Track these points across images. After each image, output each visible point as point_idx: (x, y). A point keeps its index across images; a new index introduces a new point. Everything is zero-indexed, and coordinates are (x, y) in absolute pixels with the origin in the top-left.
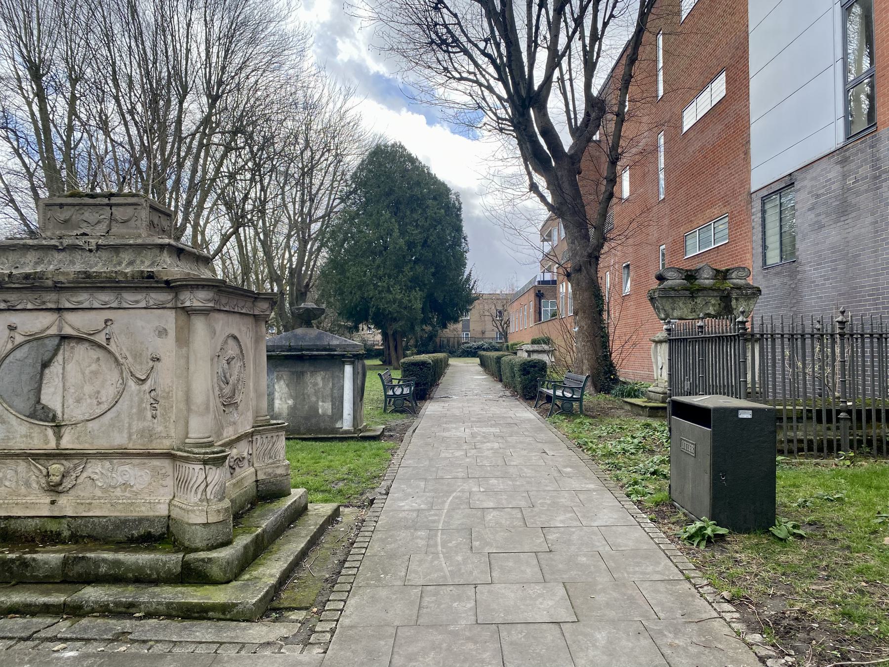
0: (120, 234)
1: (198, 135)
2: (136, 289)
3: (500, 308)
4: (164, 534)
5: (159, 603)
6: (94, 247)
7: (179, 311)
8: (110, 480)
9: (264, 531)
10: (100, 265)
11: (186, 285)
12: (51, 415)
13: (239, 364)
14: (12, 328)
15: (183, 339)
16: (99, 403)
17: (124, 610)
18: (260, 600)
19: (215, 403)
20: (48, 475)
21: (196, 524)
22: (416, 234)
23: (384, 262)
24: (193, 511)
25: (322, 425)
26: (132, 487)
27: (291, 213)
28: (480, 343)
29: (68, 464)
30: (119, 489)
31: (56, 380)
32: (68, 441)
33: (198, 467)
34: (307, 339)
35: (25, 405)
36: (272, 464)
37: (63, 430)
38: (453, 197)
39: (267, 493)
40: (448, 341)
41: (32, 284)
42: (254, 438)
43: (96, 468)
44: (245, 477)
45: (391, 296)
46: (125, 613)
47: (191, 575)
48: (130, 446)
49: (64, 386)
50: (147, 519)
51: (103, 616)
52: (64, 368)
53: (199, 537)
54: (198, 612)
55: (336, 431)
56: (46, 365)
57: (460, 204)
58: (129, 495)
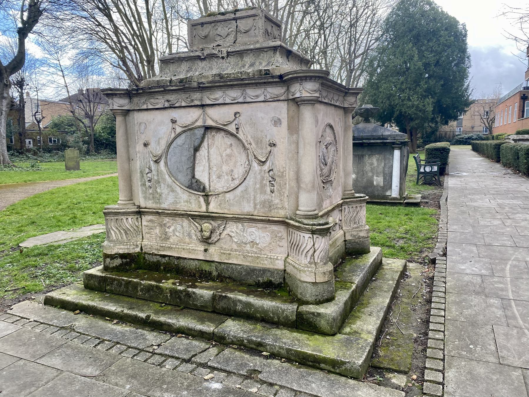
0: (244, 42)
1: (287, 8)
2: (257, 85)
3: (487, 109)
4: (281, 283)
5: (281, 348)
6: (225, 55)
7: (291, 103)
8: (242, 238)
9: (357, 287)
10: (229, 68)
11: (296, 78)
12: (202, 187)
13: (333, 149)
14: (174, 122)
15: (294, 128)
16: (233, 179)
17: (254, 347)
18: (365, 361)
19: (318, 181)
20: (202, 231)
21: (307, 282)
22: (431, 57)
23: (406, 79)
24: (304, 271)
25: (376, 193)
26: (257, 244)
27: (343, 53)
28: (470, 135)
29: (215, 224)
30: (248, 245)
31: (204, 161)
32: (213, 207)
33: (307, 236)
34: (366, 131)
35: (184, 178)
36: (356, 228)
37: (210, 198)
38: (460, 27)
39: (353, 251)
40: (446, 134)
41: (184, 87)
42: (343, 207)
43: (232, 228)
44: (336, 240)
45: (410, 103)
46: (255, 349)
47: (304, 324)
48: (255, 213)
49: (209, 166)
50: (269, 270)
51: (239, 349)
52: (208, 152)
53: (309, 293)
54: (312, 362)
55: (386, 197)
56: (197, 149)
57: (466, 31)
58: (255, 250)
